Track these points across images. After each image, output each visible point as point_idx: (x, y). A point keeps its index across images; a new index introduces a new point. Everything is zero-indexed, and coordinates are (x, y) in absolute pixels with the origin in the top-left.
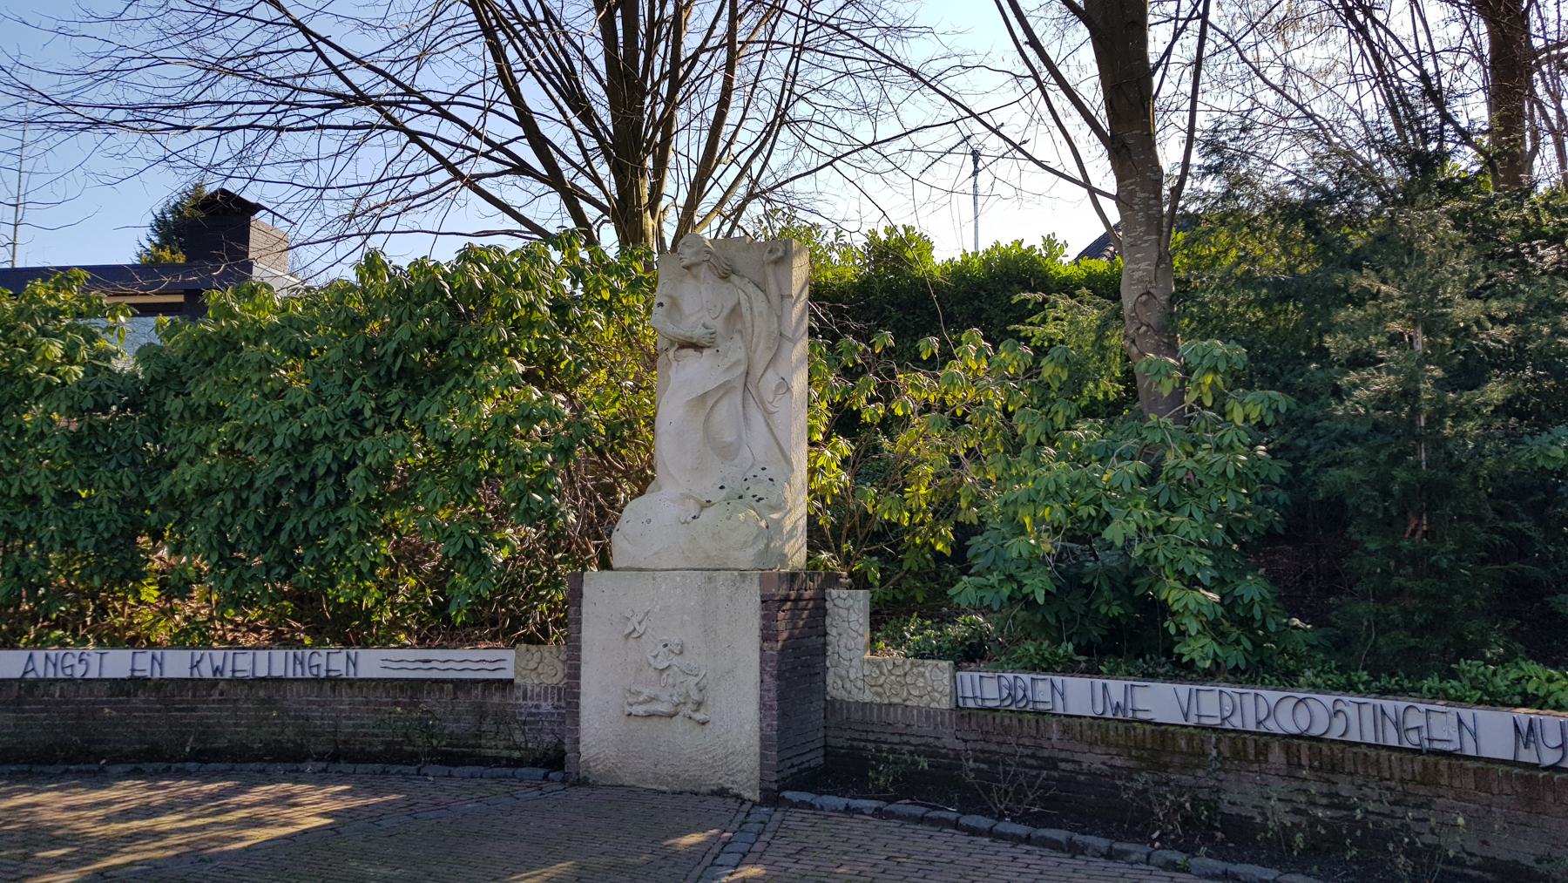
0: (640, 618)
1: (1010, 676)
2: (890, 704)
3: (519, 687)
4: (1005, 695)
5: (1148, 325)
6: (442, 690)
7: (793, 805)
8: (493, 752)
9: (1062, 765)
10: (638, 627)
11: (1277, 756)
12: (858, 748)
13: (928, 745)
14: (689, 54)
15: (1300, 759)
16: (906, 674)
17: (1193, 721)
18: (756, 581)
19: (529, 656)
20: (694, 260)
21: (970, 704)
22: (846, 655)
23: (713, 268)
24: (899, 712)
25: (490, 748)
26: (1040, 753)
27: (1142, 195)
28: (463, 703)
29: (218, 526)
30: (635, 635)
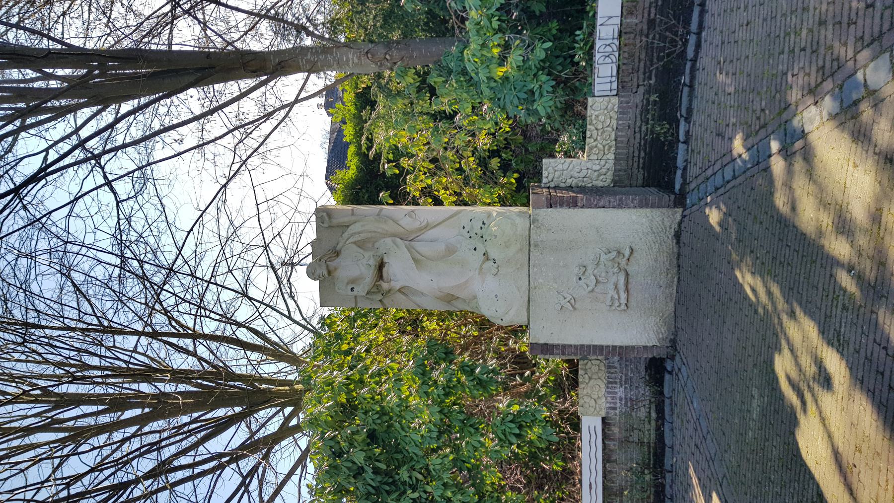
0: (562, 298)
2: (616, 140)
4: (610, 61)
5: (386, 54)
6: (610, 472)
7: (685, 183)
8: (653, 432)
9: (652, 15)
10: (568, 299)
12: (644, 163)
14: (197, 363)
16: (596, 129)
18: (538, 211)
19: (587, 405)
20: (324, 267)
21: (615, 86)
24: (620, 134)
26: (645, 32)
28: (619, 455)
30: (573, 301)
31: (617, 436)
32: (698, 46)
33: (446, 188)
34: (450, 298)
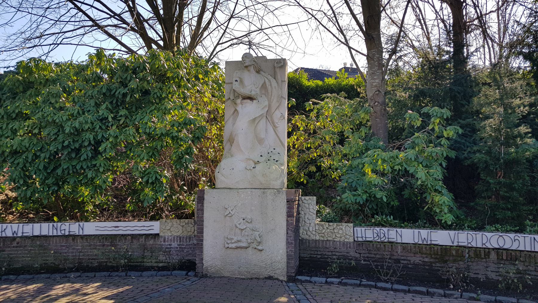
0: (232, 209)
1: (378, 229)
3: (162, 237)
5: (378, 102)
6: (126, 239)
7: (302, 282)
8: (150, 264)
10: (231, 212)
11: (493, 256)
13: (344, 256)
15: (502, 257)
17: (456, 244)
18: (285, 193)
19: (166, 224)
20: (250, 64)
21: (360, 239)
22: (308, 222)
23: (255, 68)
24: (331, 243)
25: (148, 263)
26: (393, 258)
27: (377, 56)
29: (22, 168)
30: (230, 215)
31: (148, 243)
32: (385, 289)
33: (297, 140)
34: (231, 141)
